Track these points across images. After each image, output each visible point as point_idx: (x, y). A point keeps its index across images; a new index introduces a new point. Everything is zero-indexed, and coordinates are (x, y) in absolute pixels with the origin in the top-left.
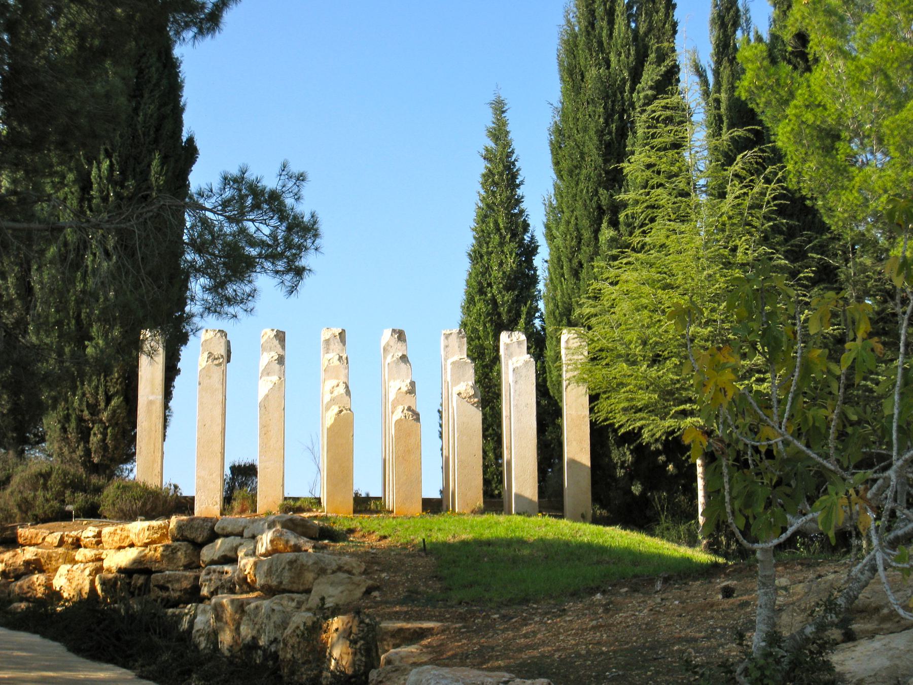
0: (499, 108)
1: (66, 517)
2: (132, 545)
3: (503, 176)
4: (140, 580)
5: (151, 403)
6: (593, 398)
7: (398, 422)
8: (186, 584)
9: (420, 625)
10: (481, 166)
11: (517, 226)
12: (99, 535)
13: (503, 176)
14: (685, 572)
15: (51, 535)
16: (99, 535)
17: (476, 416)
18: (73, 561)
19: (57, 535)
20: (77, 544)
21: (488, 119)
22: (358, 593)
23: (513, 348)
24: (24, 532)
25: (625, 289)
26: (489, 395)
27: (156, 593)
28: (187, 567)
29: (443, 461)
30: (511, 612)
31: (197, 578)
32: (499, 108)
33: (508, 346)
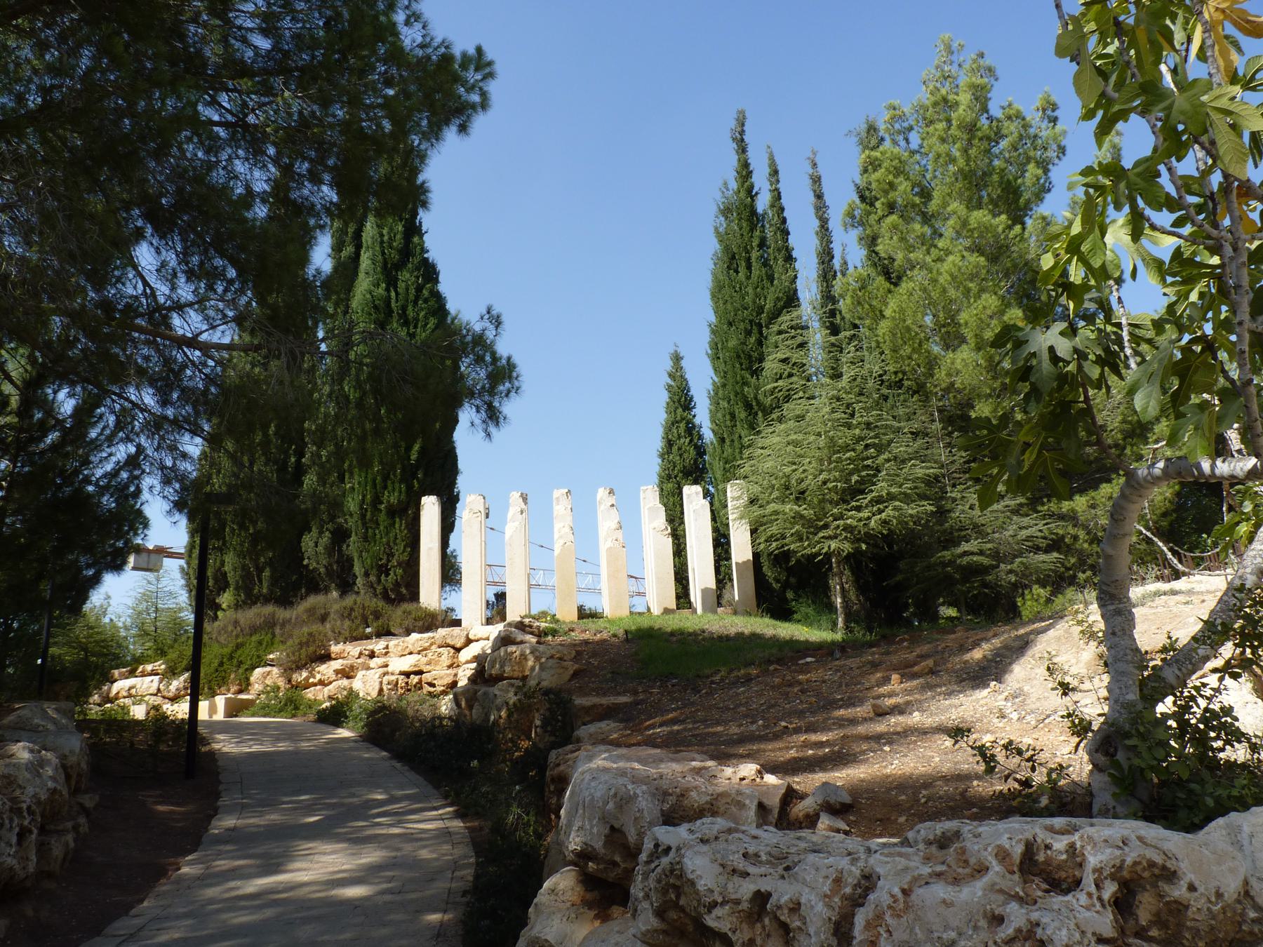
0: (677, 358)
1: (368, 637)
2: (411, 653)
3: (681, 400)
4: (414, 679)
5: (430, 549)
6: (753, 532)
7: (609, 549)
8: (449, 680)
9: (1014, 633)
10: (664, 397)
11: (692, 430)
12: (387, 647)
13: (681, 400)
14: (823, 651)
15: (353, 649)
16: (387, 647)
17: (668, 542)
18: (368, 668)
19: (358, 649)
20: (372, 655)
21: (668, 365)
22: (567, 676)
23: (693, 496)
24: (335, 649)
25: (773, 449)
26: (680, 551)
27: (427, 688)
28: (450, 667)
29: (657, 597)
30: (689, 778)
31: (456, 675)
32: (677, 358)
33: (689, 496)
